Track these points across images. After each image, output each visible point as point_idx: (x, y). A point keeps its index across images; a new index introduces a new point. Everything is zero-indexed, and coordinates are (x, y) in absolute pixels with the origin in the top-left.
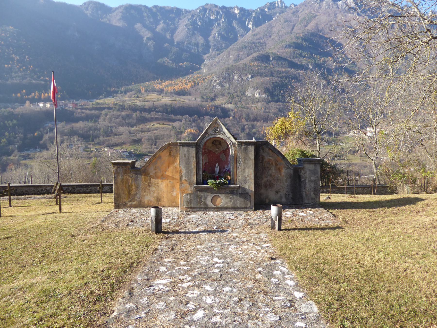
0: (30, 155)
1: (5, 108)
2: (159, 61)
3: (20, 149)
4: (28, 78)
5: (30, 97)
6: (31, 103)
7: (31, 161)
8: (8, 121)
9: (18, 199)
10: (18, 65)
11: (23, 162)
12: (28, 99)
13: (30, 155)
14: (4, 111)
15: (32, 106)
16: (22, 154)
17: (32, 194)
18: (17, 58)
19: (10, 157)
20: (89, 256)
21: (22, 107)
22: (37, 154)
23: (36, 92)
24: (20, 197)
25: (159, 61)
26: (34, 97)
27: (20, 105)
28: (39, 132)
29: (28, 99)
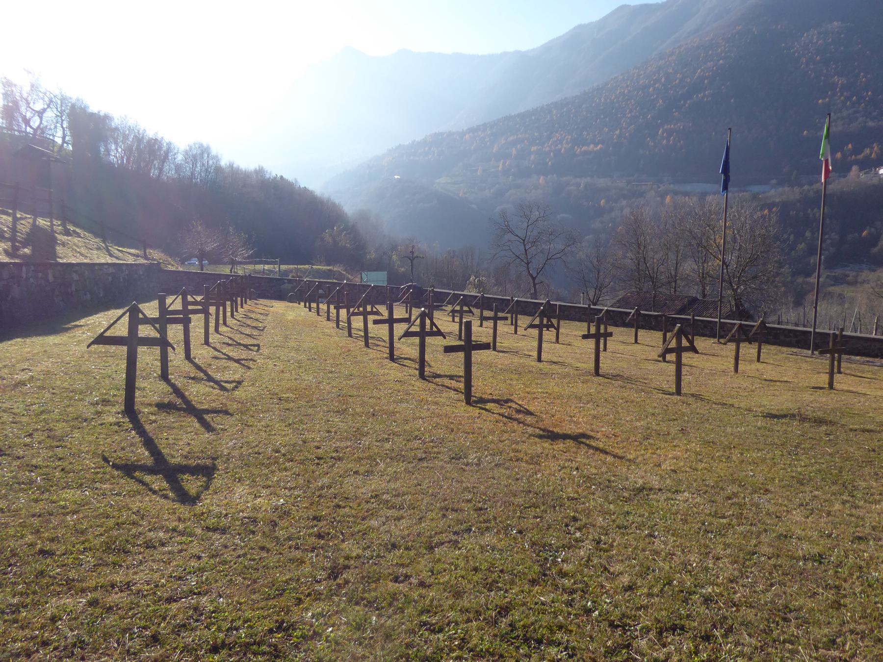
0: (848, 276)
1: (811, 184)
2: (494, 151)
3: (832, 263)
4: (860, 119)
5: (861, 157)
6: (861, 169)
7: (852, 288)
8: (812, 210)
9: (850, 361)
10: (842, 95)
11: (837, 289)
12: (856, 162)
13: (848, 276)
14: (809, 191)
15: (863, 176)
16: (833, 274)
17: (876, 356)
18: (842, 81)
19: (808, 279)
20: (687, 501)
21: (842, 180)
22: (865, 275)
23: (875, 145)
24: (853, 357)
25: (494, 151)
26: (868, 157)
27: (840, 176)
28: (873, 230)
29: (856, 162)
